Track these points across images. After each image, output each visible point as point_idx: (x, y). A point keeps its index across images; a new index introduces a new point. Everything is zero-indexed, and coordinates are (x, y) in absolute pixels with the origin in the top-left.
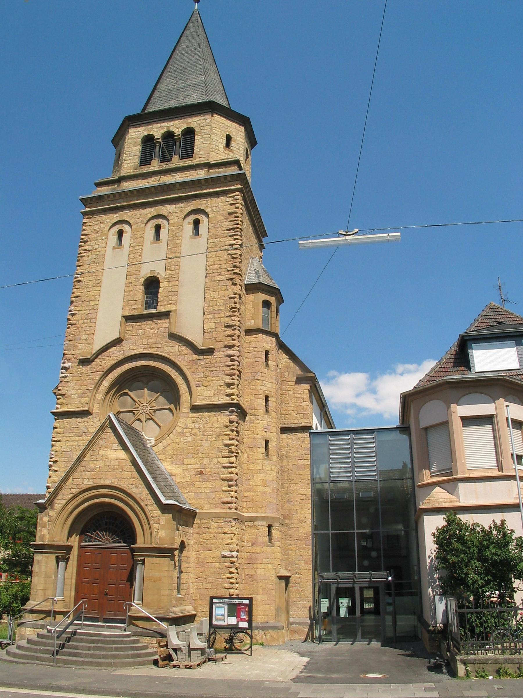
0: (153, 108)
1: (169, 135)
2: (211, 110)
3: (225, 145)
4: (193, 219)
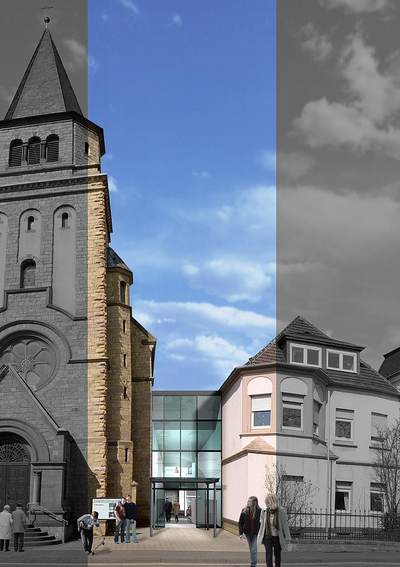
0: (18, 116)
1: (35, 140)
2: (72, 120)
3: (84, 151)
4: (62, 213)
